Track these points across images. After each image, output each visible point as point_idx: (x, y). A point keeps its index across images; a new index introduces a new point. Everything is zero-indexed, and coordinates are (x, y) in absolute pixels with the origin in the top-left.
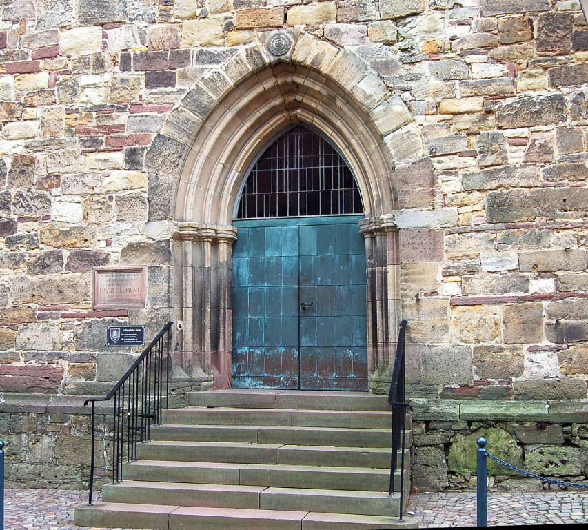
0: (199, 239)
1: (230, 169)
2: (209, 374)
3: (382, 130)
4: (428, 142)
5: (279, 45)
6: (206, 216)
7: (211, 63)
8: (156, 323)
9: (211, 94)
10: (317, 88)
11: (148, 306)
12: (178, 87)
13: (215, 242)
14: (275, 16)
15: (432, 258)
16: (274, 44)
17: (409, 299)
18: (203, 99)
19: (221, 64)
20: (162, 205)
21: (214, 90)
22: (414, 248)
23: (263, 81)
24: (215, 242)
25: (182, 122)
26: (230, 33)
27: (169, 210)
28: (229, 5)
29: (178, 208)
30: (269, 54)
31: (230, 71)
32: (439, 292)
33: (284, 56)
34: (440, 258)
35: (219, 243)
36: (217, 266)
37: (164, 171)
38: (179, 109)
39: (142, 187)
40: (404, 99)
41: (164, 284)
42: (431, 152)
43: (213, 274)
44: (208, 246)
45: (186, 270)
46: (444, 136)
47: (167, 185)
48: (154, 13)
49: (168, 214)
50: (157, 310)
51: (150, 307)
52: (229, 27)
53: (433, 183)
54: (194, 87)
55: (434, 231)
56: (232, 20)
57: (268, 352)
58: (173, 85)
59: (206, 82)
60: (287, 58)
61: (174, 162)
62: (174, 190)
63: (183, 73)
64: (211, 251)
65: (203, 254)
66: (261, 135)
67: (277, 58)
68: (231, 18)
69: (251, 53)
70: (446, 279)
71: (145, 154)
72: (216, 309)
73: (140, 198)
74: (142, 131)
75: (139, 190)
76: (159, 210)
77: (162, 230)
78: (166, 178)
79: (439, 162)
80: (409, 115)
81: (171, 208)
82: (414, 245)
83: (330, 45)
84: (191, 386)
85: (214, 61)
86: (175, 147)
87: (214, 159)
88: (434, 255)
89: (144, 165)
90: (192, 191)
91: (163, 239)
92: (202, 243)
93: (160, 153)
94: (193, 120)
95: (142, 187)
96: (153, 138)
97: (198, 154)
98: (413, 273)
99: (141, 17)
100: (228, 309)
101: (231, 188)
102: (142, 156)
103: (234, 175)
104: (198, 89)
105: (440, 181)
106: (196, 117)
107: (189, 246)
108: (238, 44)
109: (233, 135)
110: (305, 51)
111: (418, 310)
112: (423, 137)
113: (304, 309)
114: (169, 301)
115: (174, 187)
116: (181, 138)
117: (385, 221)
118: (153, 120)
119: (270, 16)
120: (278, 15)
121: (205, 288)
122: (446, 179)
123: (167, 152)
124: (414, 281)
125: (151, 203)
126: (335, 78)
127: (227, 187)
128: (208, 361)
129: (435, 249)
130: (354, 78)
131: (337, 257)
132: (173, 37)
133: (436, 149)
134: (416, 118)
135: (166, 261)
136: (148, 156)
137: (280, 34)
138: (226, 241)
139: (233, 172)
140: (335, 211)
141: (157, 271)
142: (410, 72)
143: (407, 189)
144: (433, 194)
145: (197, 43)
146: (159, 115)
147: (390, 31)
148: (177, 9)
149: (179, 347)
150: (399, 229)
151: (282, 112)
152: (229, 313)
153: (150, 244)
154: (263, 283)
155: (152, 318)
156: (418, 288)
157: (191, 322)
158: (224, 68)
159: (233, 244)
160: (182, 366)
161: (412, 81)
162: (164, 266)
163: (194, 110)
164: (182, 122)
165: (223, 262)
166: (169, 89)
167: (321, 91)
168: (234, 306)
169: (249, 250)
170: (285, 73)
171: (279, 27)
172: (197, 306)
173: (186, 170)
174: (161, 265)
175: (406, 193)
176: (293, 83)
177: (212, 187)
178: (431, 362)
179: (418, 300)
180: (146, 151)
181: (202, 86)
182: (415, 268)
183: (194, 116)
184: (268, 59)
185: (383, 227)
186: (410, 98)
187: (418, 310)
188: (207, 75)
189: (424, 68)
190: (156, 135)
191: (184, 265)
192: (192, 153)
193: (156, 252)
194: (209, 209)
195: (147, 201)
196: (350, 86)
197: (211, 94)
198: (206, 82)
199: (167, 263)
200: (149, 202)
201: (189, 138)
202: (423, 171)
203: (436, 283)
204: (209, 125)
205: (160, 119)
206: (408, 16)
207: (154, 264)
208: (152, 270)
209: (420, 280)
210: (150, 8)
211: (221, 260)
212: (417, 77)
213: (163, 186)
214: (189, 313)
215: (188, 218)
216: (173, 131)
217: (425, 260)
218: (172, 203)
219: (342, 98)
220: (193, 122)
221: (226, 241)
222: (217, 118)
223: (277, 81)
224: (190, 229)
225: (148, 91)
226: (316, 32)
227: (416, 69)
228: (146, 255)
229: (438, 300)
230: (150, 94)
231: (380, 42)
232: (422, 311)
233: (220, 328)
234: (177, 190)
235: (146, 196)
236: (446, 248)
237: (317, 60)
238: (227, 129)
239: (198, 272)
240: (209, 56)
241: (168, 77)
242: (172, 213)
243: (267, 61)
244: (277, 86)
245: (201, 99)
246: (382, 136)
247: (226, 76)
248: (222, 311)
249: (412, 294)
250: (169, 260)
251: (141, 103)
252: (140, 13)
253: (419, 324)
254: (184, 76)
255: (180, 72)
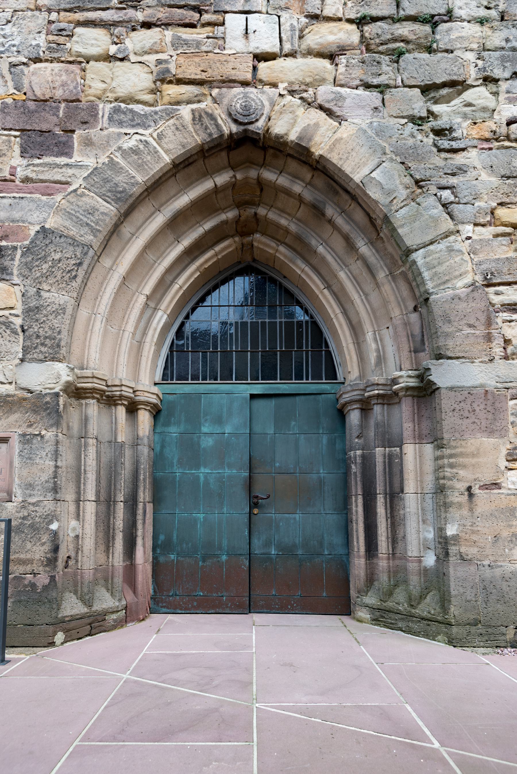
0: (109, 400)
1: (155, 309)
2: (120, 600)
3: (410, 241)
4: (480, 263)
5: (246, 108)
6: (120, 368)
7: (133, 126)
8: (32, 526)
9: (133, 173)
10: (297, 188)
11: (18, 498)
12: (76, 157)
13: (132, 409)
14: (238, 66)
15: (490, 432)
16: (238, 106)
17: (457, 494)
18: (120, 179)
19: (150, 130)
20: (46, 338)
21: (140, 167)
22: (462, 417)
23: (214, 174)
24: (132, 409)
25: (84, 211)
26: (165, 86)
27: (58, 346)
28: (163, 44)
29: (76, 349)
30: (229, 120)
31: (166, 140)
32: (503, 485)
33: (253, 126)
34: (502, 433)
35: (138, 409)
36: (136, 443)
37: (51, 285)
38: (79, 192)
39: (12, 308)
40: (442, 199)
41: (47, 462)
42: (486, 279)
43: (128, 453)
44: (121, 412)
45: (86, 445)
46: (505, 256)
47: (57, 306)
48: (38, 45)
49: (57, 353)
50: (33, 504)
51: (21, 499)
52: (164, 78)
53: (489, 323)
54: (104, 159)
55: (493, 393)
56: (169, 66)
57: (204, 561)
58: (69, 155)
59: (124, 153)
60: (259, 129)
61: (69, 271)
62: (68, 316)
63: (87, 139)
64: (126, 420)
65: (114, 423)
66: (202, 265)
67: (242, 128)
68: (166, 61)
69: (200, 116)
70: (511, 465)
71: (18, 256)
72: (132, 503)
73: (8, 324)
74: (13, 221)
75: (6, 313)
76: (43, 344)
77: (47, 377)
78: (56, 296)
79: (497, 294)
80: (448, 225)
81: (63, 343)
82: (462, 413)
83: (327, 117)
84: (90, 624)
85: (138, 124)
86: (71, 248)
87: (134, 287)
88: (493, 429)
89: (15, 272)
90: (98, 326)
91: (48, 391)
92: (113, 408)
93: (45, 257)
94: (102, 209)
95: (12, 308)
96: (32, 233)
97: (108, 272)
98: (461, 455)
99: (15, 49)
100: (149, 502)
101: (156, 336)
102: (12, 259)
103: (161, 318)
104: (112, 164)
105: (499, 321)
106: (108, 205)
107: (92, 408)
108: (178, 103)
109: (161, 256)
110: (290, 122)
111: (471, 510)
112: (472, 255)
113: (254, 503)
114: (55, 489)
115: (69, 310)
116: (82, 236)
117: (401, 380)
118: (32, 206)
119: (230, 65)
120: (245, 65)
121: (115, 471)
122: (508, 318)
123: (57, 256)
124: (464, 466)
125: (27, 333)
126: (335, 161)
127: (151, 333)
128: (119, 580)
129: (495, 419)
130: (365, 164)
131: (302, 436)
132: (69, 82)
133: (492, 274)
134: (460, 227)
135: (52, 426)
136: (23, 260)
137: (247, 93)
138: (149, 408)
139: (160, 313)
140: (299, 377)
141: (35, 441)
142: (450, 162)
143: (450, 330)
144: (489, 338)
145: (111, 96)
146: (44, 198)
147: (419, 105)
148: (77, 42)
149: (71, 563)
150: (438, 388)
151: (232, 236)
152: (150, 507)
153: (25, 399)
154: (199, 469)
155: (24, 518)
156: (471, 477)
157: (93, 524)
158: (155, 135)
159: (156, 412)
160: (76, 593)
161: (453, 175)
162: (49, 435)
163: (104, 195)
164: (84, 211)
165: (144, 436)
166: (62, 160)
167: (304, 193)
168: (157, 500)
169: (179, 423)
170: (247, 164)
171: (245, 84)
172: (102, 499)
173: (89, 293)
174: (43, 432)
175: (447, 335)
176: (260, 183)
177: (130, 328)
178: (494, 591)
179: (471, 495)
180: (19, 252)
181: (119, 159)
182: (464, 447)
183: (105, 203)
184: (229, 128)
185: (370, 397)
186: (452, 198)
187: (471, 510)
188: (132, 143)
189: (473, 157)
190: (37, 228)
191: (83, 436)
192: (98, 269)
193: (35, 412)
194: (123, 359)
195: (19, 330)
196: (358, 176)
197: (133, 173)
198: (124, 153)
199: (54, 429)
200: (23, 331)
201: (95, 236)
202: (474, 305)
203: (498, 471)
204: (126, 229)
205: (47, 204)
206: (444, 85)
207: (30, 430)
208: (26, 439)
209: (473, 465)
210: (31, 36)
211: (141, 433)
212: (461, 170)
213: (49, 308)
214: (90, 509)
215: (91, 365)
216: (68, 223)
217: (479, 435)
218: (64, 335)
219: (335, 204)
220: (102, 213)
221: (149, 408)
222: (141, 220)
223: (235, 176)
224: (95, 380)
225: (25, 162)
226: (305, 95)
227: (459, 159)
228: (16, 416)
229: (502, 496)
230: (29, 165)
231: (403, 117)
232: (476, 514)
233: (136, 530)
234: (74, 317)
235: (18, 322)
236: (511, 419)
237: (307, 134)
238: (151, 244)
239: (104, 448)
240: (130, 116)
241: (60, 142)
242: (63, 351)
243: (226, 131)
244: (233, 185)
245: (118, 179)
246: (408, 252)
247: (159, 148)
248: (140, 506)
249: (462, 486)
250: (57, 424)
251: (13, 177)
252: (13, 42)
253: (473, 532)
254: (88, 143)
255: (81, 136)
